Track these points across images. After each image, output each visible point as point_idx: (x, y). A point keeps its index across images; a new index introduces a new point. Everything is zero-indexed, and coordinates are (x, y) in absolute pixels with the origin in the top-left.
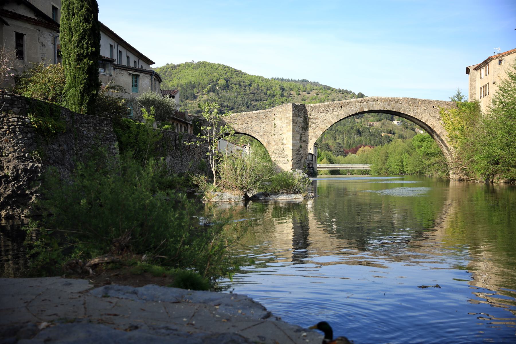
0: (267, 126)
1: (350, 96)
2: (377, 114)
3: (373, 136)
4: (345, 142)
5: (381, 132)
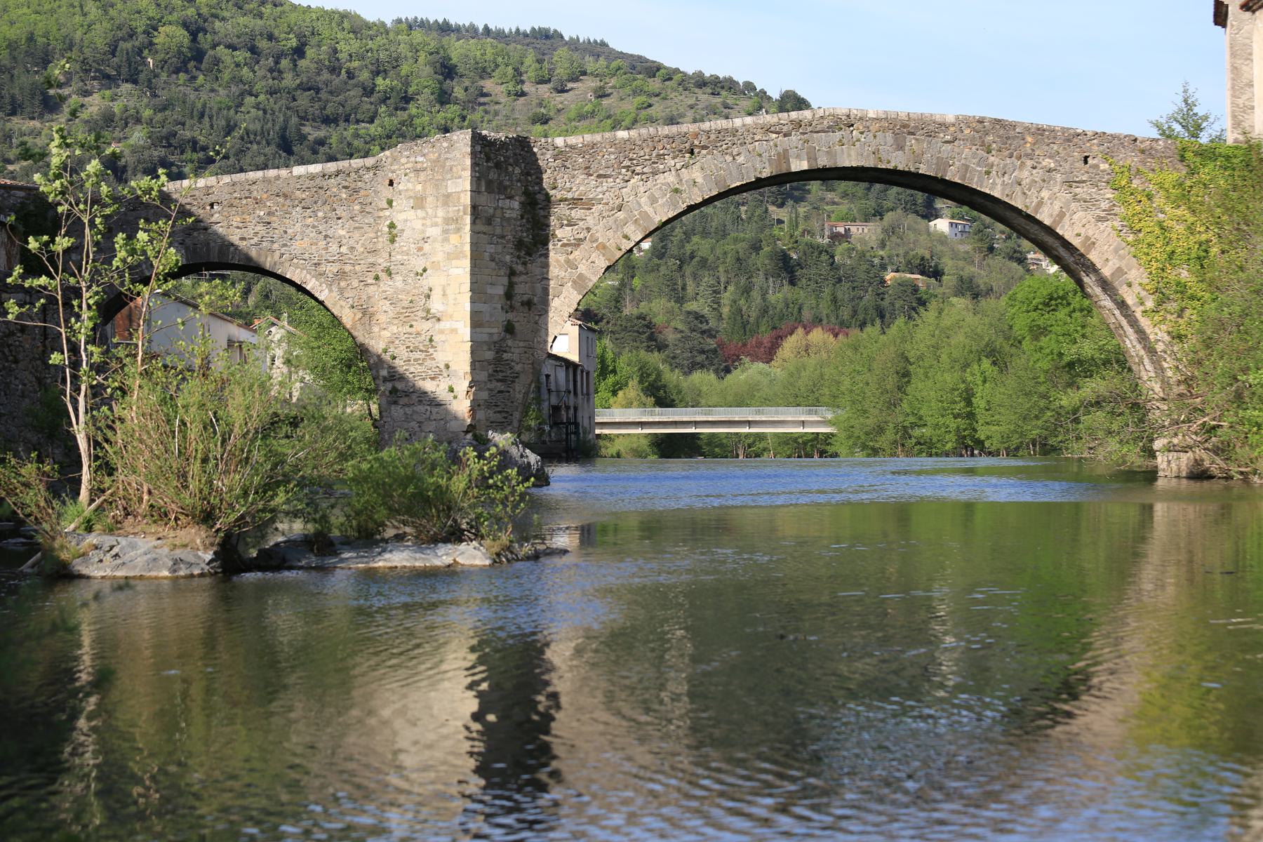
0: (356, 235)
1: (746, 104)
2: (866, 185)
3: (846, 286)
4: (725, 311)
5: (883, 267)
